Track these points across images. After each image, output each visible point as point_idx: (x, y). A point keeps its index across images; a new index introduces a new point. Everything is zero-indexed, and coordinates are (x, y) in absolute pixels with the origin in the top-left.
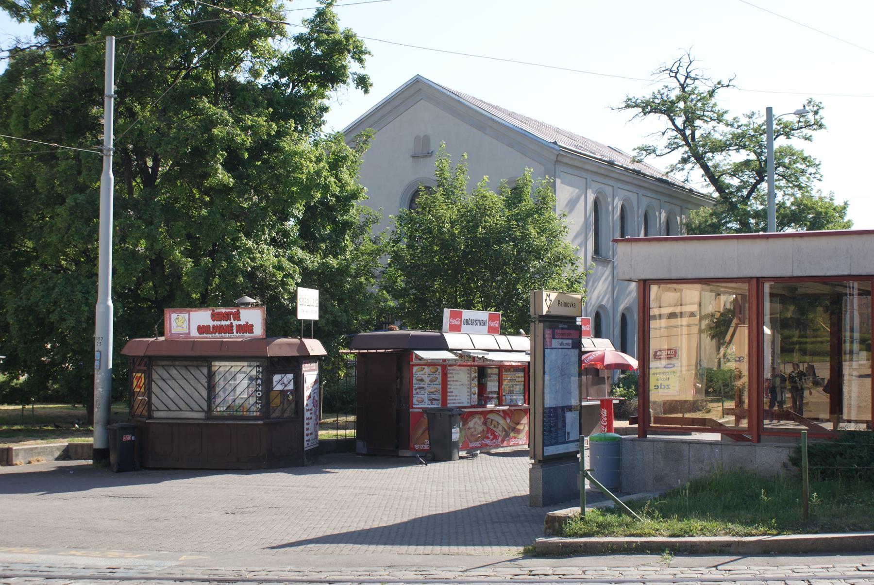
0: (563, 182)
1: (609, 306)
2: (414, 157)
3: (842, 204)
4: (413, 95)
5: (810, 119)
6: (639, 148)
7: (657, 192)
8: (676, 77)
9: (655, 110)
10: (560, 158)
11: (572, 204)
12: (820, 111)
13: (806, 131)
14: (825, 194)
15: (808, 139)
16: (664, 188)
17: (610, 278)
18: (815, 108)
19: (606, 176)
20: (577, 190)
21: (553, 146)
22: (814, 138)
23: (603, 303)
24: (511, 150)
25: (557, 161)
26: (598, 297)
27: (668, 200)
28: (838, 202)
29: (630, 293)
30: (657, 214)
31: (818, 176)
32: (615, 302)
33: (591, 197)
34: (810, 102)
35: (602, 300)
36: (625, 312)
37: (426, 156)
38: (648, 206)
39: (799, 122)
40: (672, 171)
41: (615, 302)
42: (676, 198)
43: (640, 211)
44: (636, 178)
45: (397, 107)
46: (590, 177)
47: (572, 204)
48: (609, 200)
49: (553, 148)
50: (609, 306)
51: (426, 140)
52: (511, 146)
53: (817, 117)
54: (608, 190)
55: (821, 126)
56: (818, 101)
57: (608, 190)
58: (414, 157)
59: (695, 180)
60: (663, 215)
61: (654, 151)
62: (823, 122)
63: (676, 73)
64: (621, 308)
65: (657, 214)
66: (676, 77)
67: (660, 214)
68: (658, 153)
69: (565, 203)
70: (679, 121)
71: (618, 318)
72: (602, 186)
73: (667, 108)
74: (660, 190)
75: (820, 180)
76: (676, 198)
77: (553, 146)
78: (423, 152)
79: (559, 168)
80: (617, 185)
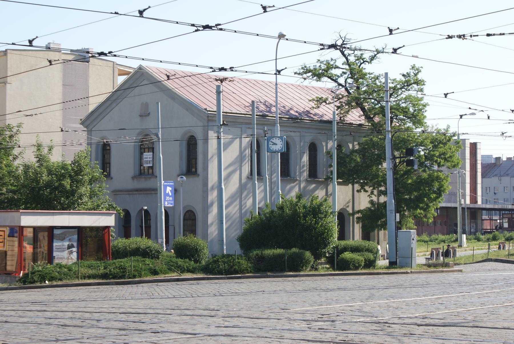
2: (140, 116)
10: (210, 118)
52: (187, 110)
65: (324, 144)
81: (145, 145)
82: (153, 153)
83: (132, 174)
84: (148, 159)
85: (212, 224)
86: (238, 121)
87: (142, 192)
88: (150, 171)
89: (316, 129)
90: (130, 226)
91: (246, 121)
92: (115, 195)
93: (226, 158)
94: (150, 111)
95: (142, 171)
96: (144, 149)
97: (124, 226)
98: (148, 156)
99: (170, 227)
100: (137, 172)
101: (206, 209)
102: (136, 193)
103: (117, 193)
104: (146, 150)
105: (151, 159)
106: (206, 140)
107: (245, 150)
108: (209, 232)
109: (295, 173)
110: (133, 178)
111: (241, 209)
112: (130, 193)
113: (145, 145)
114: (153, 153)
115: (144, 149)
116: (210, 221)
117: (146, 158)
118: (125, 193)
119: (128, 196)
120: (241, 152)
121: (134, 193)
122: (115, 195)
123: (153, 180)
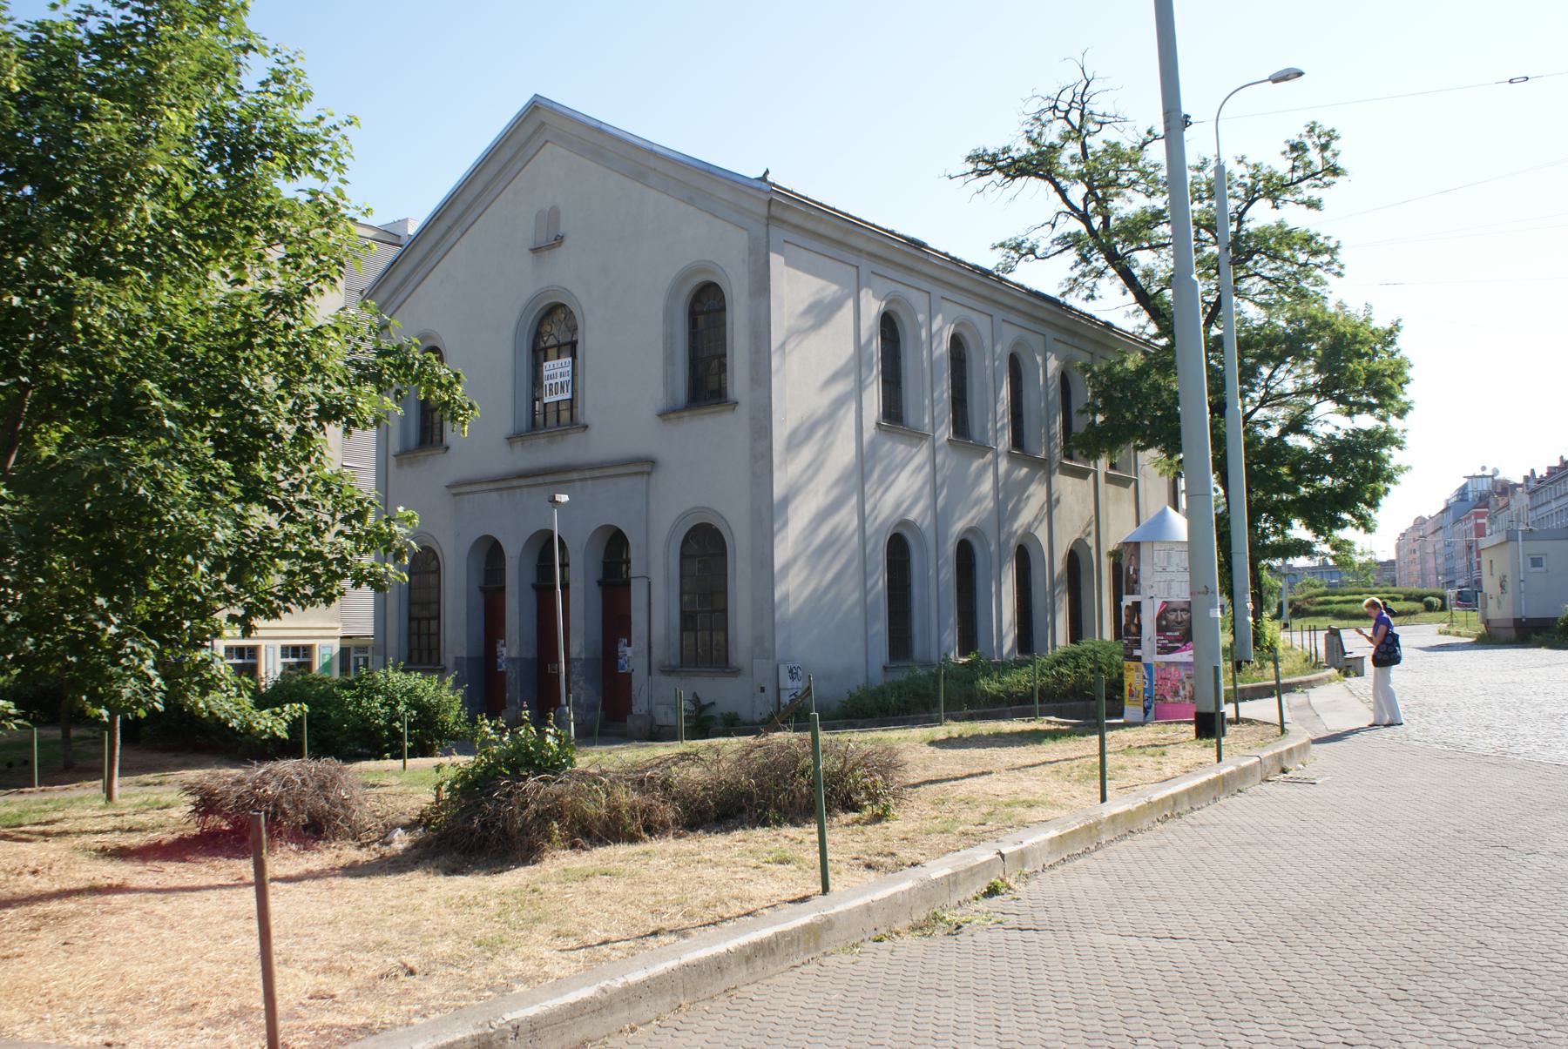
0: (789, 263)
1: (926, 523)
2: (535, 250)
3: (1388, 326)
4: (531, 136)
5: (1314, 161)
6: (1002, 245)
7: (1036, 319)
8: (1066, 118)
9: (1022, 172)
10: (775, 211)
11: (821, 313)
12: (1334, 145)
13: (1307, 190)
14: (1356, 308)
15: (1313, 204)
16: (1050, 314)
17: (927, 468)
18: (1323, 140)
19: (910, 269)
20: (834, 287)
21: (758, 184)
22: (1325, 203)
23: (912, 516)
24: (691, 209)
25: (770, 218)
26: (898, 506)
27: (1064, 337)
28: (1381, 322)
29: (979, 501)
30: (1039, 359)
31: (1335, 267)
32: (941, 519)
33: (872, 308)
34: (1312, 130)
35: (909, 510)
36: (970, 538)
37: (550, 247)
38: (1017, 344)
39: (1293, 169)
40: (1071, 290)
41: (941, 519)
42: (1082, 337)
43: (998, 348)
44: (984, 286)
45: (509, 161)
46: (865, 264)
47: (821, 313)
48: (921, 317)
49: (759, 189)
50: (926, 523)
51: (552, 216)
52: (690, 201)
53: (1328, 154)
54: (918, 300)
55: (1335, 171)
56: (1327, 128)
57: (918, 300)
58: (535, 250)
59: (1113, 305)
60: (1053, 364)
61: (1032, 251)
62: (1340, 162)
63: (1067, 112)
64: (958, 527)
65: (1039, 359)
66: (1066, 118)
67: (1045, 360)
68: (1039, 252)
69: (801, 307)
70: (1077, 192)
71: (950, 549)
72: (901, 288)
73: (1039, 165)
74: (1040, 314)
75: (1339, 274)
76: (1082, 337)
77: (758, 184)
78: (549, 243)
79: (777, 233)
80: (938, 291)
81: (551, 329)
82: (574, 356)
83: (508, 428)
84: (559, 380)
85: (787, 567)
86: (853, 241)
87: (540, 480)
88: (565, 416)
89: (1025, 314)
90: (503, 589)
91: (871, 248)
92: (455, 495)
93: (810, 352)
94: (563, 229)
95: (539, 418)
96: (546, 350)
97: (482, 589)
98: (556, 369)
99: (633, 582)
100: (524, 423)
101: (767, 515)
102: (522, 482)
103: (464, 489)
104: (552, 352)
105: (568, 378)
106: (761, 286)
107: (869, 342)
108: (778, 595)
109: (984, 429)
110: (511, 440)
111: (863, 519)
112: (503, 484)
113: (551, 329)
114: (574, 356)
115: (546, 350)
116: (781, 556)
117: (551, 377)
118: (485, 487)
119: (494, 495)
120: (859, 349)
121: (515, 483)
122: (455, 495)
123: (574, 438)
